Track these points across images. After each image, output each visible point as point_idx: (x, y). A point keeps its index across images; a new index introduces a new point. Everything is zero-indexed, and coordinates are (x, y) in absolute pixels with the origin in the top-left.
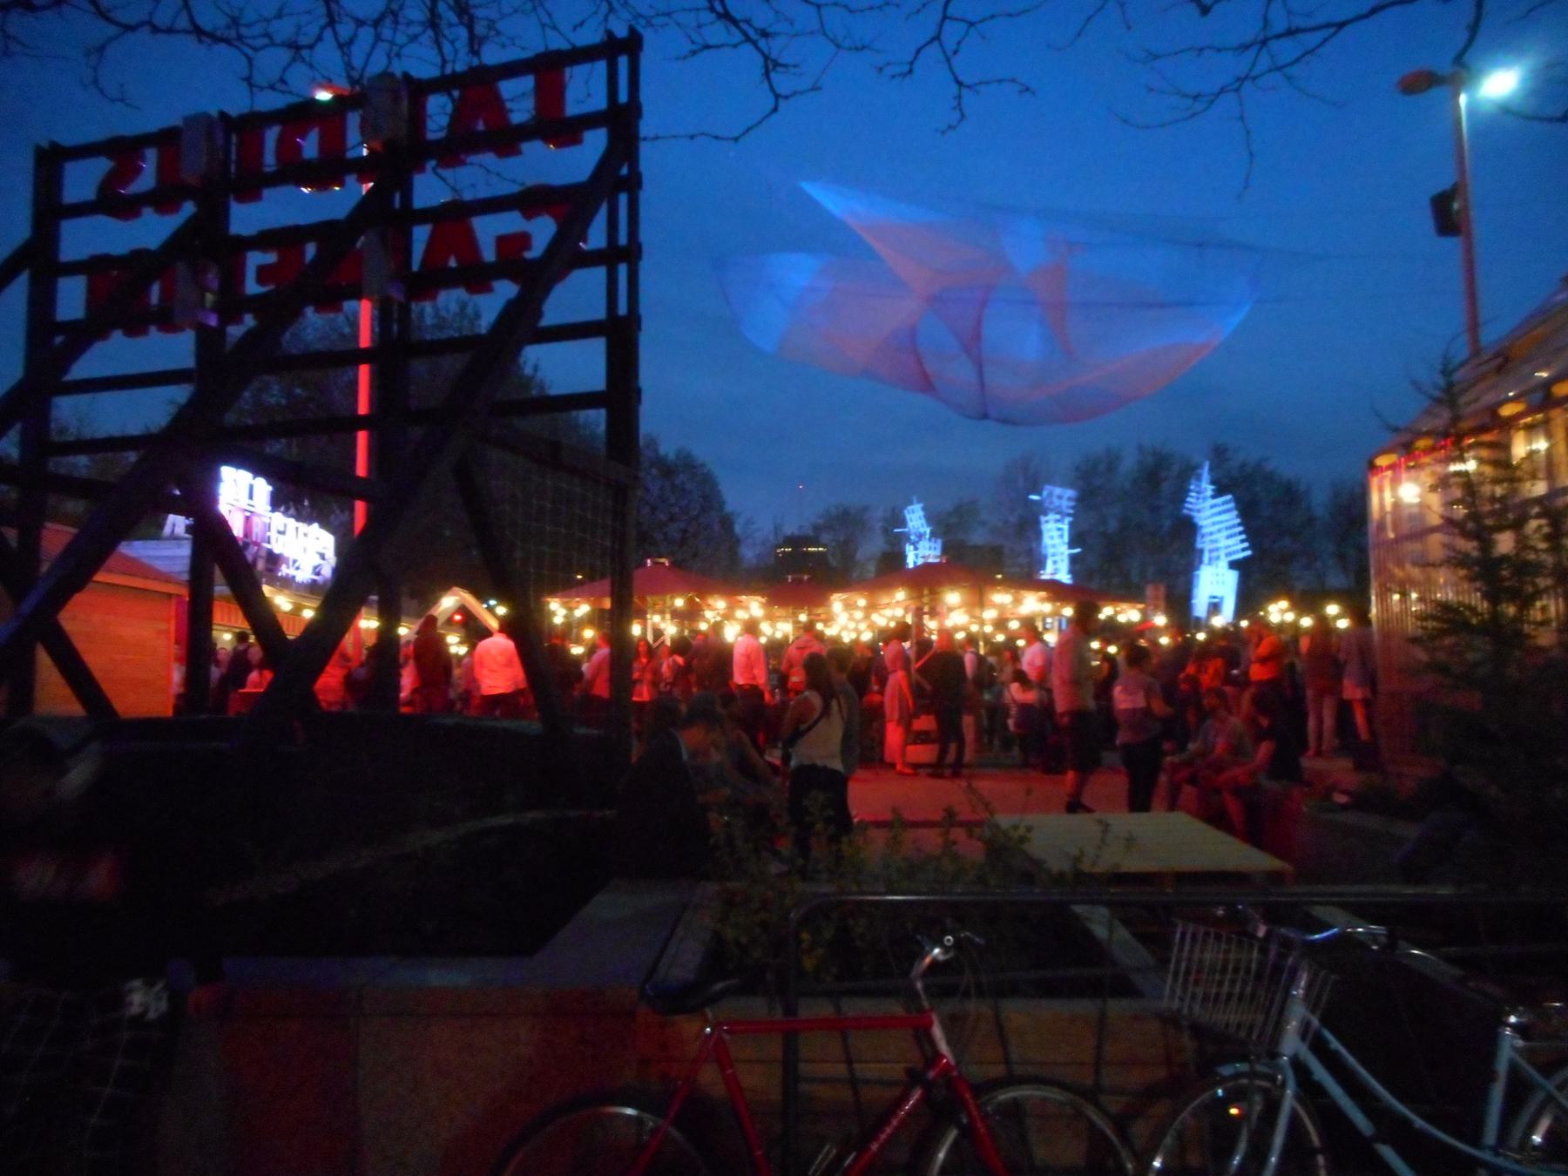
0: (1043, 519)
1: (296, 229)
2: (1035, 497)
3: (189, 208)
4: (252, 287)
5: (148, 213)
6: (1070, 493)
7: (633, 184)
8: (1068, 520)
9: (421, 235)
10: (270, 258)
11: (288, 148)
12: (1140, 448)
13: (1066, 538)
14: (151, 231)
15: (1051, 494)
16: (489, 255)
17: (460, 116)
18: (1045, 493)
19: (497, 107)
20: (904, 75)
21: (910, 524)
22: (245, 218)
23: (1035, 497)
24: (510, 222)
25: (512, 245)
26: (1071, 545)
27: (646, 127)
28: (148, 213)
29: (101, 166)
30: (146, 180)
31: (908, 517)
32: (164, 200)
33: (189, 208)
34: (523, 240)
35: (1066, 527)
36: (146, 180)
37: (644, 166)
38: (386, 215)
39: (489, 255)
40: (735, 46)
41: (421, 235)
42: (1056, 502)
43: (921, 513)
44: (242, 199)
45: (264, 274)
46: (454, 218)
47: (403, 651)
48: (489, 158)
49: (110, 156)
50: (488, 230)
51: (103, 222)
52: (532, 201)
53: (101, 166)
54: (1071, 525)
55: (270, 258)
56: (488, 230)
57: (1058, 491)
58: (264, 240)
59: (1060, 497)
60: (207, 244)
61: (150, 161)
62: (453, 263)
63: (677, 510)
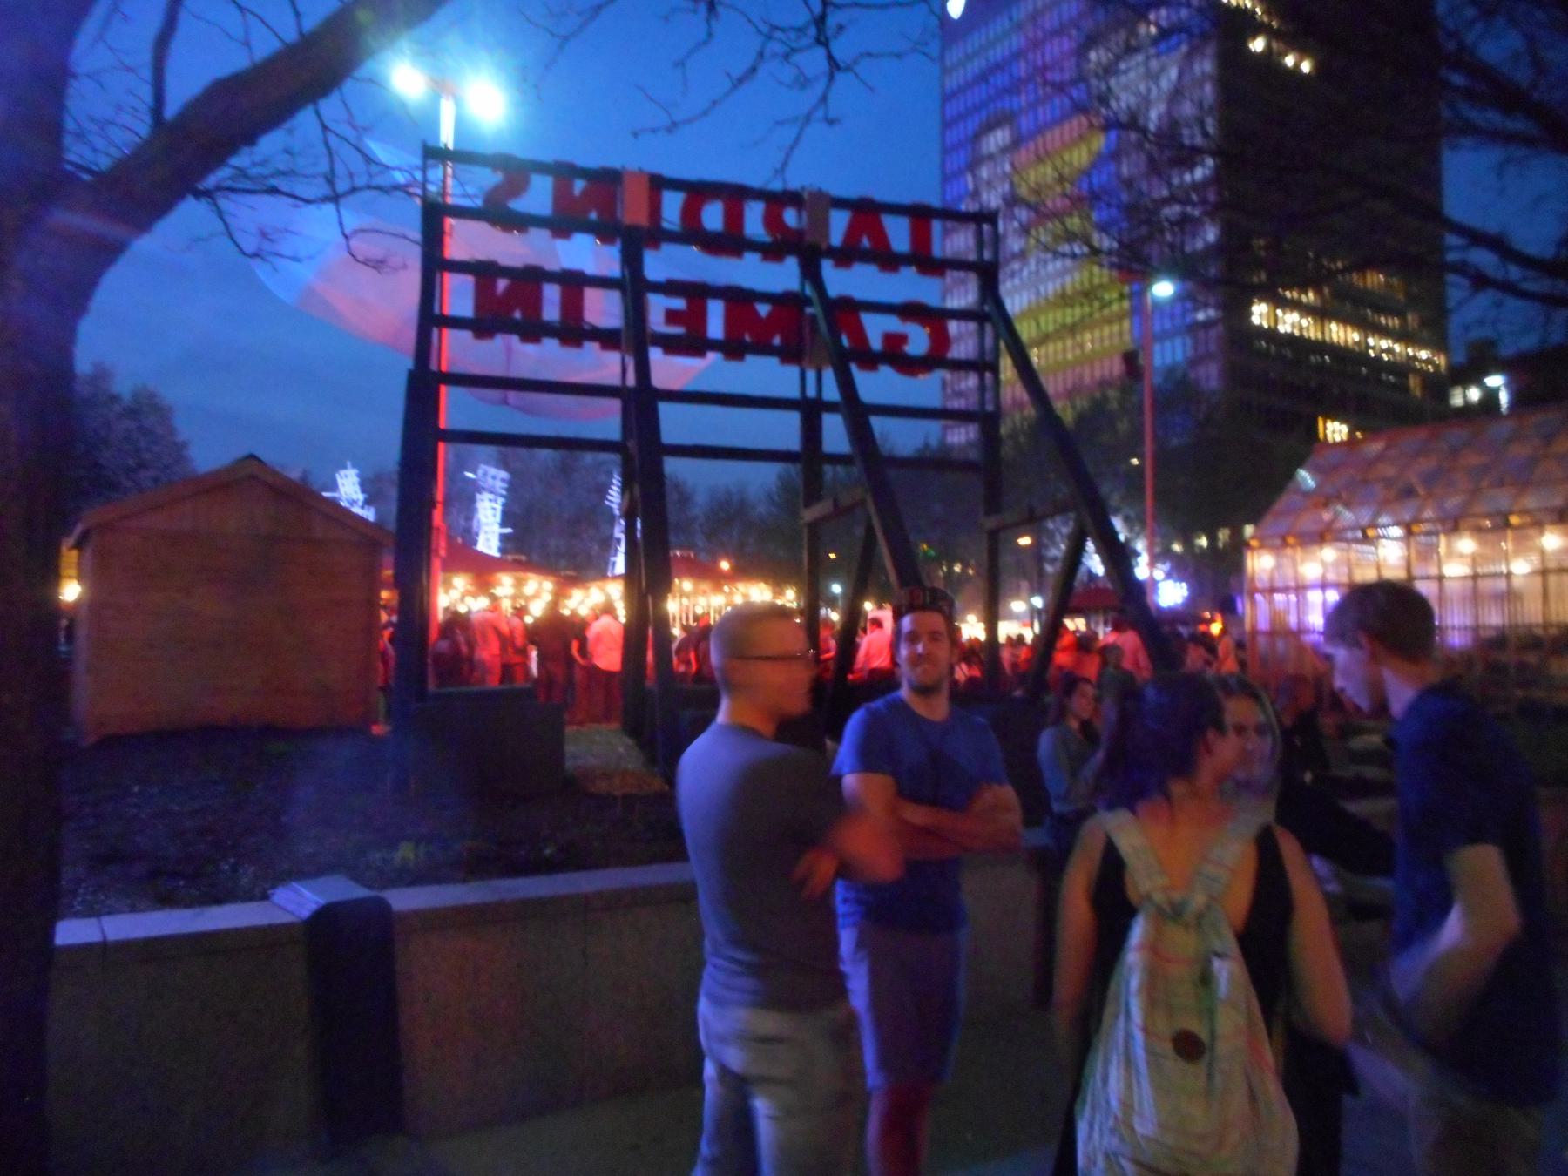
0: (479, 496)
2: (470, 475)
6: (504, 474)
8: (501, 500)
10: (679, 304)
11: (691, 213)
13: (498, 518)
15: (485, 474)
16: (876, 343)
17: (852, 233)
18: (480, 472)
20: (705, 43)
21: (342, 489)
23: (470, 475)
24: (893, 324)
25: (894, 342)
26: (503, 524)
31: (340, 481)
35: (499, 507)
39: (876, 343)
40: (781, 83)
42: (490, 481)
43: (356, 480)
47: (73, 572)
50: (876, 328)
52: (911, 311)
54: (504, 505)
55: (679, 304)
57: (493, 471)
58: (670, 288)
59: (494, 478)
63: (147, 456)
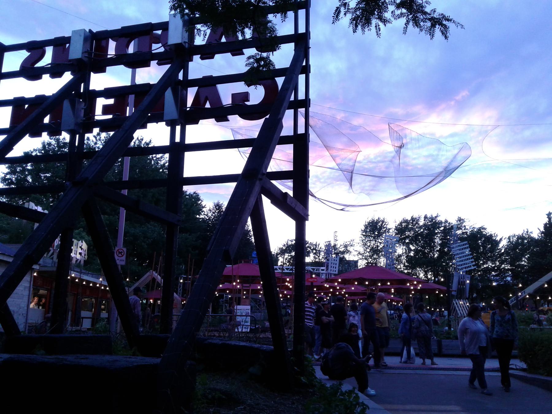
1: (106, 32)
3: (68, 77)
4: (99, 115)
5: (46, 77)
7: (306, 70)
9: (191, 94)
10: (111, 101)
12: (426, 217)
14: (49, 86)
16: (227, 101)
19: (216, 98)
22: (98, 81)
24: (240, 87)
25: (240, 99)
27: (312, 42)
28: (46, 77)
29: (24, 54)
30: (47, 60)
32: (55, 71)
33: (68, 77)
34: (245, 96)
36: (47, 60)
37: (311, 62)
38: (174, 83)
41: (191, 94)
44: (96, 72)
45: (106, 109)
46: (209, 83)
48: (211, 122)
49: (28, 50)
50: (226, 93)
51: (21, 81)
53: (24, 54)
55: (111, 101)
56: (226, 93)
58: (107, 93)
60: (77, 98)
61: (49, 52)
62: (208, 105)
